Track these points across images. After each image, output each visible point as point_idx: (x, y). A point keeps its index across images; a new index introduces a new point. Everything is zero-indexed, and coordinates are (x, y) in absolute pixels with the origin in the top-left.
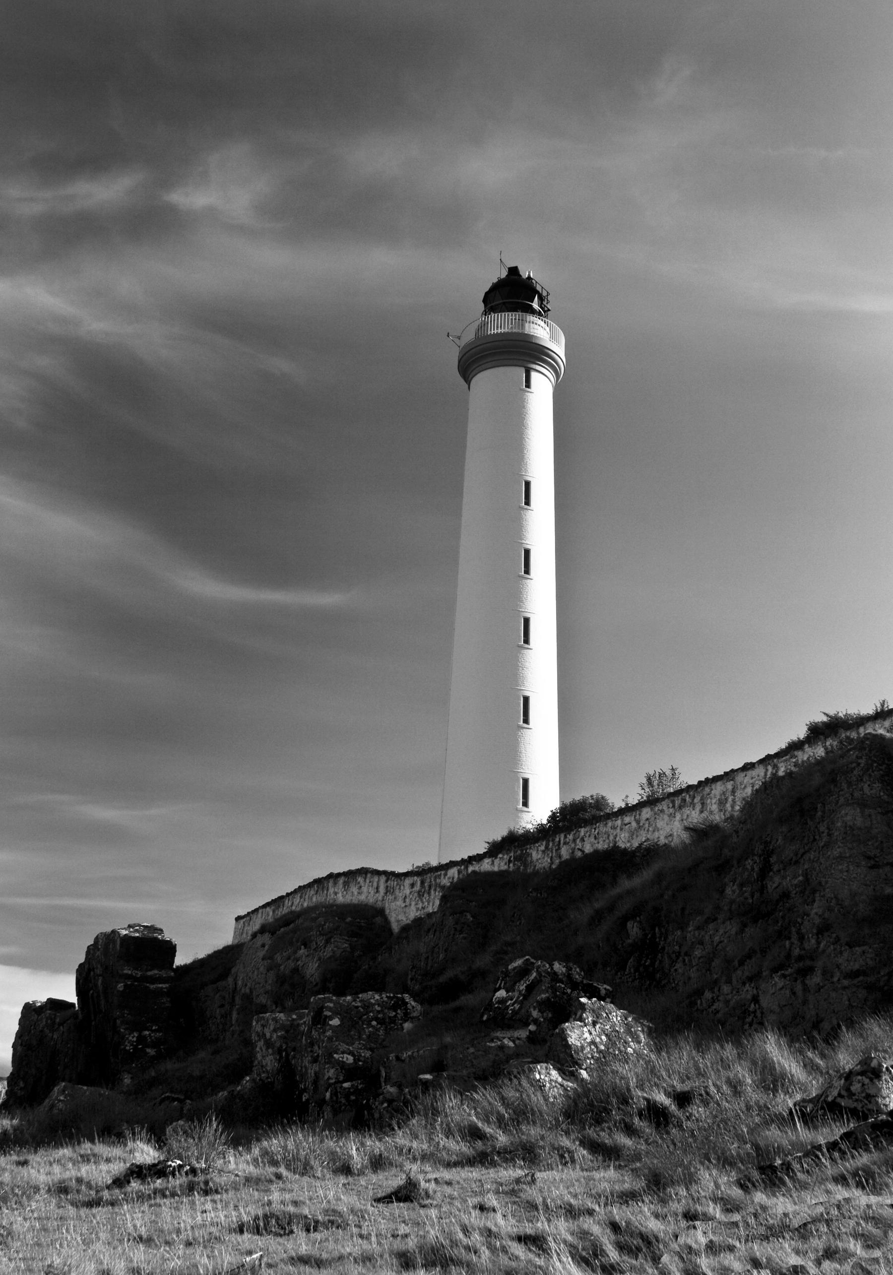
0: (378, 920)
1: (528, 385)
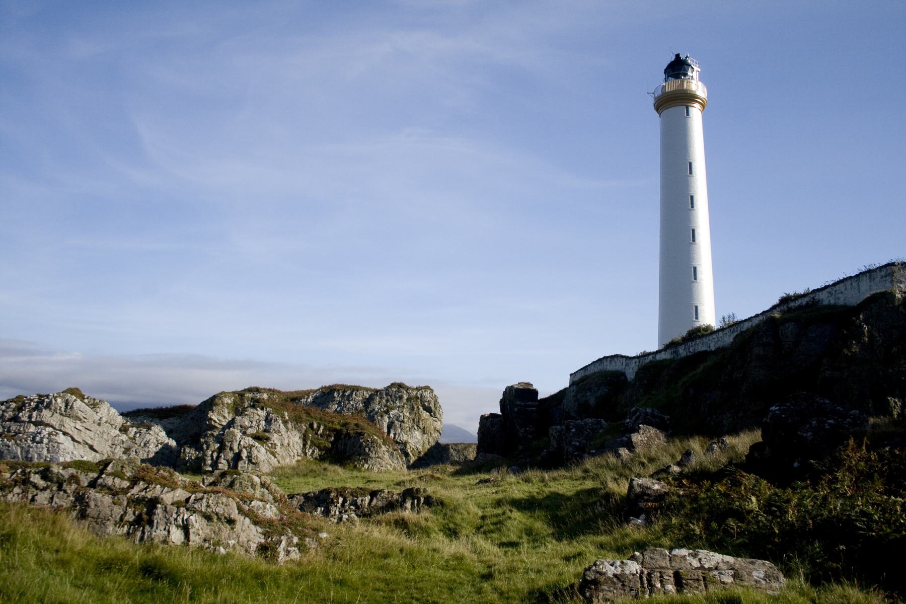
0: (623, 378)
1: (688, 114)
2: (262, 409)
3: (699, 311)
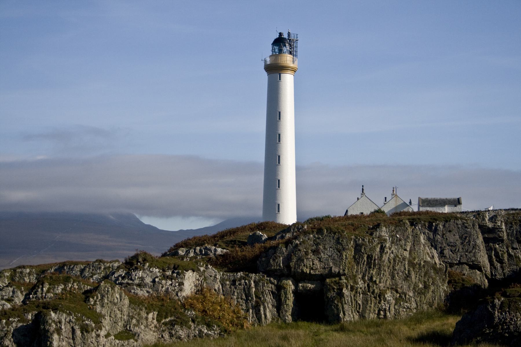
2: (11, 287)
3: (280, 207)
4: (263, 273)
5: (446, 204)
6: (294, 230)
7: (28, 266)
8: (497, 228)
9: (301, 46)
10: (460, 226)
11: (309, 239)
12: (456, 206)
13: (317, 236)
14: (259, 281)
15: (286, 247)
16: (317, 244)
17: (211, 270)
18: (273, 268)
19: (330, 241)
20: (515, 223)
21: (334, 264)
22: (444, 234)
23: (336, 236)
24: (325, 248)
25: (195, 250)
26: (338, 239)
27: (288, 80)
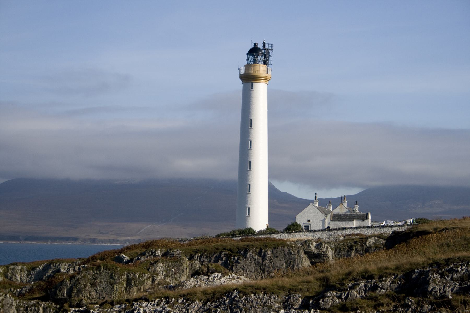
4: (52, 301)
5: (355, 219)
6: (148, 253)
7: (20, 263)
8: (322, 254)
9: (275, 56)
10: (286, 252)
11: (89, 274)
12: (363, 221)
13: (95, 272)
14: (47, 308)
15: (70, 281)
16: (95, 279)
17: (8, 299)
18: (58, 297)
19: (106, 276)
20: (344, 248)
21: (107, 294)
22: (271, 259)
23: (110, 272)
24: (101, 282)
25: (74, 268)
26: (112, 274)
27: (261, 91)
